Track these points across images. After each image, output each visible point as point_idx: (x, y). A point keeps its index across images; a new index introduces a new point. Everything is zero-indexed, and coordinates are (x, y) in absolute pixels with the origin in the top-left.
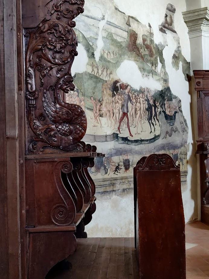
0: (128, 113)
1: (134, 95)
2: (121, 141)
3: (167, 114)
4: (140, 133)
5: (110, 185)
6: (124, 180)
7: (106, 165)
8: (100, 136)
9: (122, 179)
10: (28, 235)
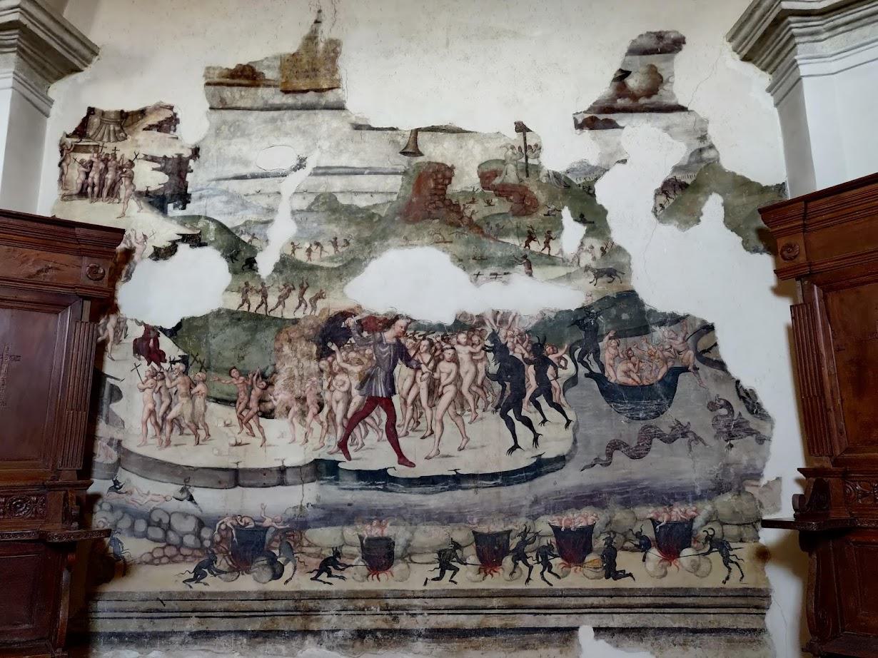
1: (425, 343)
2: (351, 482)
3: (612, 381)
4: (456, 453)
5: (294, 613)
6: (361, 603)
7: (277, 552)
8: (265, 471)
9: (353, 596)
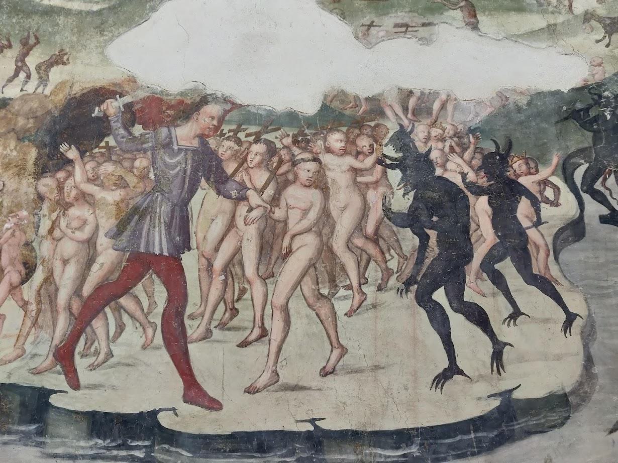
0: (189, 260)
4: (315, 381)
10: (448, 155)
